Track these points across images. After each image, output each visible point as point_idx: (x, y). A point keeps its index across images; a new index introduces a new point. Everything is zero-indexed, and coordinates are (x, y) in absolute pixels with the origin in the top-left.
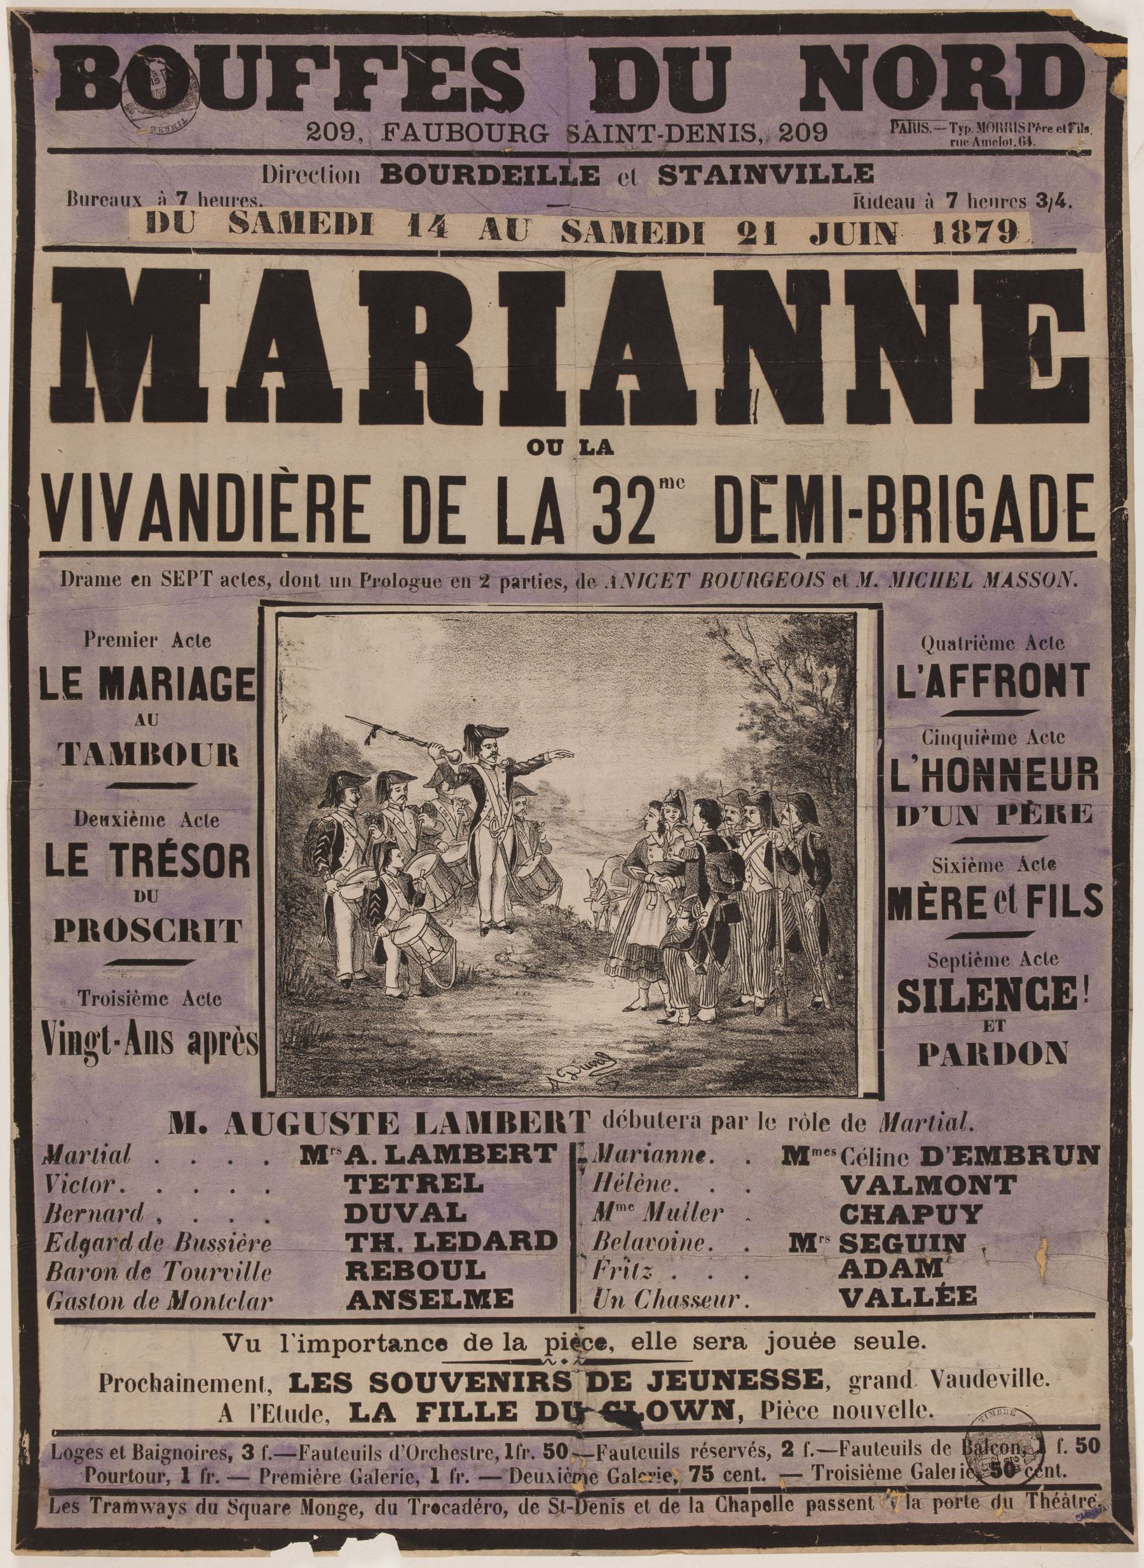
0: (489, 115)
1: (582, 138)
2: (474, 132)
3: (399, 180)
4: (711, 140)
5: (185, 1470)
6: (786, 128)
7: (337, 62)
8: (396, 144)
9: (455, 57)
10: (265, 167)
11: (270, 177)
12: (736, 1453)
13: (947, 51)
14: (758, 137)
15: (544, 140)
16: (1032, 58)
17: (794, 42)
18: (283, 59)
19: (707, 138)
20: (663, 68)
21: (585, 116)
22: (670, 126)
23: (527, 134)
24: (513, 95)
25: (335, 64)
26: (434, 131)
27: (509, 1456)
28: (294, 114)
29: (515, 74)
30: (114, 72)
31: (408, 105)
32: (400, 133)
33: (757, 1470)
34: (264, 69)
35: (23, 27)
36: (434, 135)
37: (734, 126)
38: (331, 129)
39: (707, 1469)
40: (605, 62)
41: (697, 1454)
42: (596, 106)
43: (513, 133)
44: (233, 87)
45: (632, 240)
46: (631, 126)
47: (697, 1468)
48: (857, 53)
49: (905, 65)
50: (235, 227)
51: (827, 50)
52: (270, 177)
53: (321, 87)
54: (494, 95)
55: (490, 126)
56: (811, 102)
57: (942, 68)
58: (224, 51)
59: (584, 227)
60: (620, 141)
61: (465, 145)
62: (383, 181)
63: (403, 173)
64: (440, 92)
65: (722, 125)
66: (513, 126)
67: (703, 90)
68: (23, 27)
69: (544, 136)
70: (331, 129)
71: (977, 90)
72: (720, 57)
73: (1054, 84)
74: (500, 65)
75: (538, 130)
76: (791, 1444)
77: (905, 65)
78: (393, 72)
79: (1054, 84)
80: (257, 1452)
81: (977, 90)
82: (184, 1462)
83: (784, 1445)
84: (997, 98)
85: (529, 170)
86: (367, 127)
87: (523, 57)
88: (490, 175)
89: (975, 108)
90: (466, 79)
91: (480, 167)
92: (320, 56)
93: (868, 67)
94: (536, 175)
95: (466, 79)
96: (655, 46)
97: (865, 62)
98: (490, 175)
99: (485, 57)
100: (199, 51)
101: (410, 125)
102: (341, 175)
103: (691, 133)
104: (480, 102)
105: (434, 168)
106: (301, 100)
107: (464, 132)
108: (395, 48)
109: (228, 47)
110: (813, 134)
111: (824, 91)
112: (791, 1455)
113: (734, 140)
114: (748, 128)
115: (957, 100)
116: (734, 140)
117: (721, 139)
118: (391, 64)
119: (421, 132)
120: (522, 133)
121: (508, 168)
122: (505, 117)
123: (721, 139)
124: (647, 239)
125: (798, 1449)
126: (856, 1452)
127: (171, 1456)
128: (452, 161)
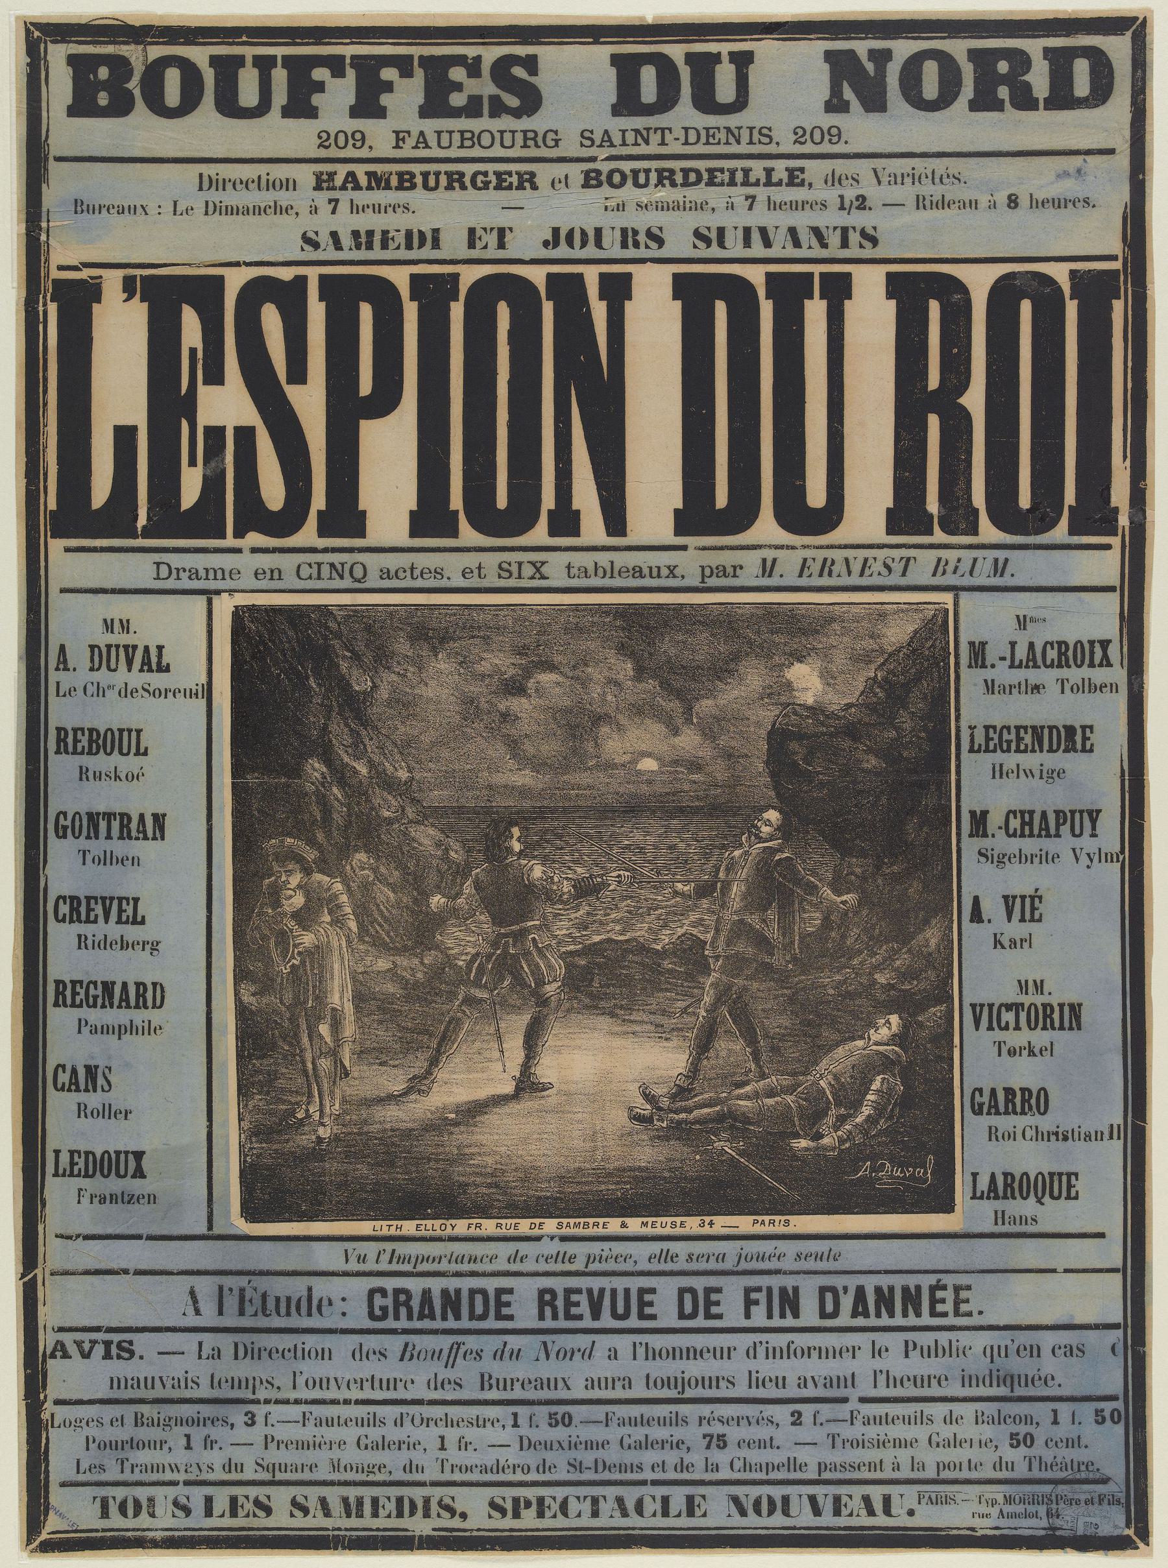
0: (506, 122)
1: (598, 142)
2: (486, 140)
3: (600, 185)
4: (727, 143)
5: (188, 1437)
6: (324, 136)
7: (421, 70)
8: (407, 152)
9: (474, 68)
10: (201, 175)
11: (206, 185)
12: (744, 1422)
13: (973, 54)
14: (774, 141)
15: (557, 145)
16: (1060, 61)
17: (818, 47)
18: (299, 68)
19: (723, 140)
20: (685, 73)
21: (603, 121)
22: (686, 129)
23: (540, 139)
24: (531, 101)
25: (351, 73)
26: (445, 138)
27: (515, 1425)
28: (303, 122)
29: (532, 79)
30: (128, 80)
31: (426, 112)
32: (411, 142)
33: (771, 1439)
34: (280, 76)
35: (39, 37)
36: (445, 143)
37: (751, 129)
38: (341, 137)
39: (721, 1437)
40: (627, 68)
41: (704, 1422)
42: (616, 111)
43: (526, 139)
44: (248, 95)
45: (370, 246)
46: (648, 129)
47: (712, 1436)
48: (881, 58)
49: (931, 69)
50: (313, 236)
51: (852, 53)
52: (206, 185)
53: (338, 94)
54: (513, 101)
55: (502, 132)
56: (836, 105)
57: (968, 71)
58: (239, 61)
59: (324, 239)
60: (636, 144)
61: (477, 152)
62: (583, 187)
63: (603, 178)
64: (457, 100)
65: (739, 128)
66: (525, 132)
67: (725, 90)
68: (39, 37)
69: (557, 141)
70: (341, 137)
71: (1003, 92)
72: (743, 61)
73: (1082, 86)
74: (519, 72)
75: (551, 136)
76: (800, 1414)
77: (931, 69)
78: (338, 81)
79: (1082, 86)
80: (260, 1419)
81: (1003, 92)
82: (187, 1430)
83: (792, 1415)
84: (1024, 100)
85: (733, 172)
86: (379, 136)
87: (541, 64)
88: (692, 177)
89: (1002, 110)
90: (486, 87)
91: (682, 170)
92: (336, 66)
93: (893, 71)
94: (739, 176)
95: (486, 87)
96: (199, 55)
97: (890, 65)
98: (692, 177)
99: (501, 68)
100: (214, 61)
101: (422, 133)
102: (278, 183)
103: (708, 136)
104: (497, 108)
105: (635, 173)
106: (317, 108)
107: (475, 139)
108: (344, 57)
109: (719, 53)
110: (351, 142)
111: (848, 94)
112: (800, 1424)
113: (751, 143)
114: (765, 131)
115: (984, 102)
116: (751, 143)
117: (738, 142)
118: (406, 73)
119: (432, 140)
120: (534, 139)
121: (711, 171)
122: (525, 123)
123: (738, 142)
124: (384, 246)
125: (807, 1418)
126: (867, 1422)
127: (173, 1422)
128: (443, 167)
